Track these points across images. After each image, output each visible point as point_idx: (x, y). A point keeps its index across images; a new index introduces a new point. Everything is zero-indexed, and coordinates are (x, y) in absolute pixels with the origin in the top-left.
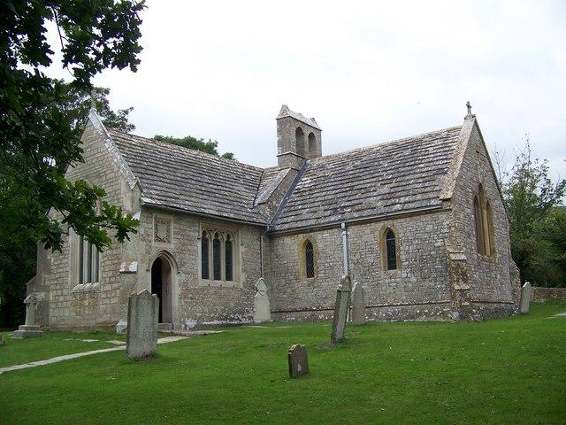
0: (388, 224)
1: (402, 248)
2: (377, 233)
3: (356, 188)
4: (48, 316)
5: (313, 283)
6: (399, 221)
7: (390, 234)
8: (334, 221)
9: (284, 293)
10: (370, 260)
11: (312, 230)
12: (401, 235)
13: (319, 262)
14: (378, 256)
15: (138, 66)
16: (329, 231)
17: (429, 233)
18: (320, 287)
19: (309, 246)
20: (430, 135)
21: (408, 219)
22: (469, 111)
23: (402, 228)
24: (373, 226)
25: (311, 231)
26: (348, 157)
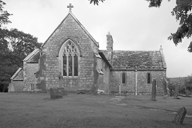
0: (149, 72)
1: (152, 78)
2: (146, 74)
3: (121, 61)
4: (45, 86)
5: (125, 85)
6: (152, 71)
7: (149, 74)
8: (133, 69)
9: (115, 87)
10: (143, 80)
11: (125, 71)
12: (152, 75)
13: (128, 80)
14: (145, 80)
15: (72, 5)
16: (131, 71)
17: (160, 76)
18: (127, 86)
19: (149, 74)
20: (133, 52)
21: (155, 72)
22: (161, 48)
23: (152, 73)
24: (144, 72)
25: (125, 71)
26: (127, 52)
